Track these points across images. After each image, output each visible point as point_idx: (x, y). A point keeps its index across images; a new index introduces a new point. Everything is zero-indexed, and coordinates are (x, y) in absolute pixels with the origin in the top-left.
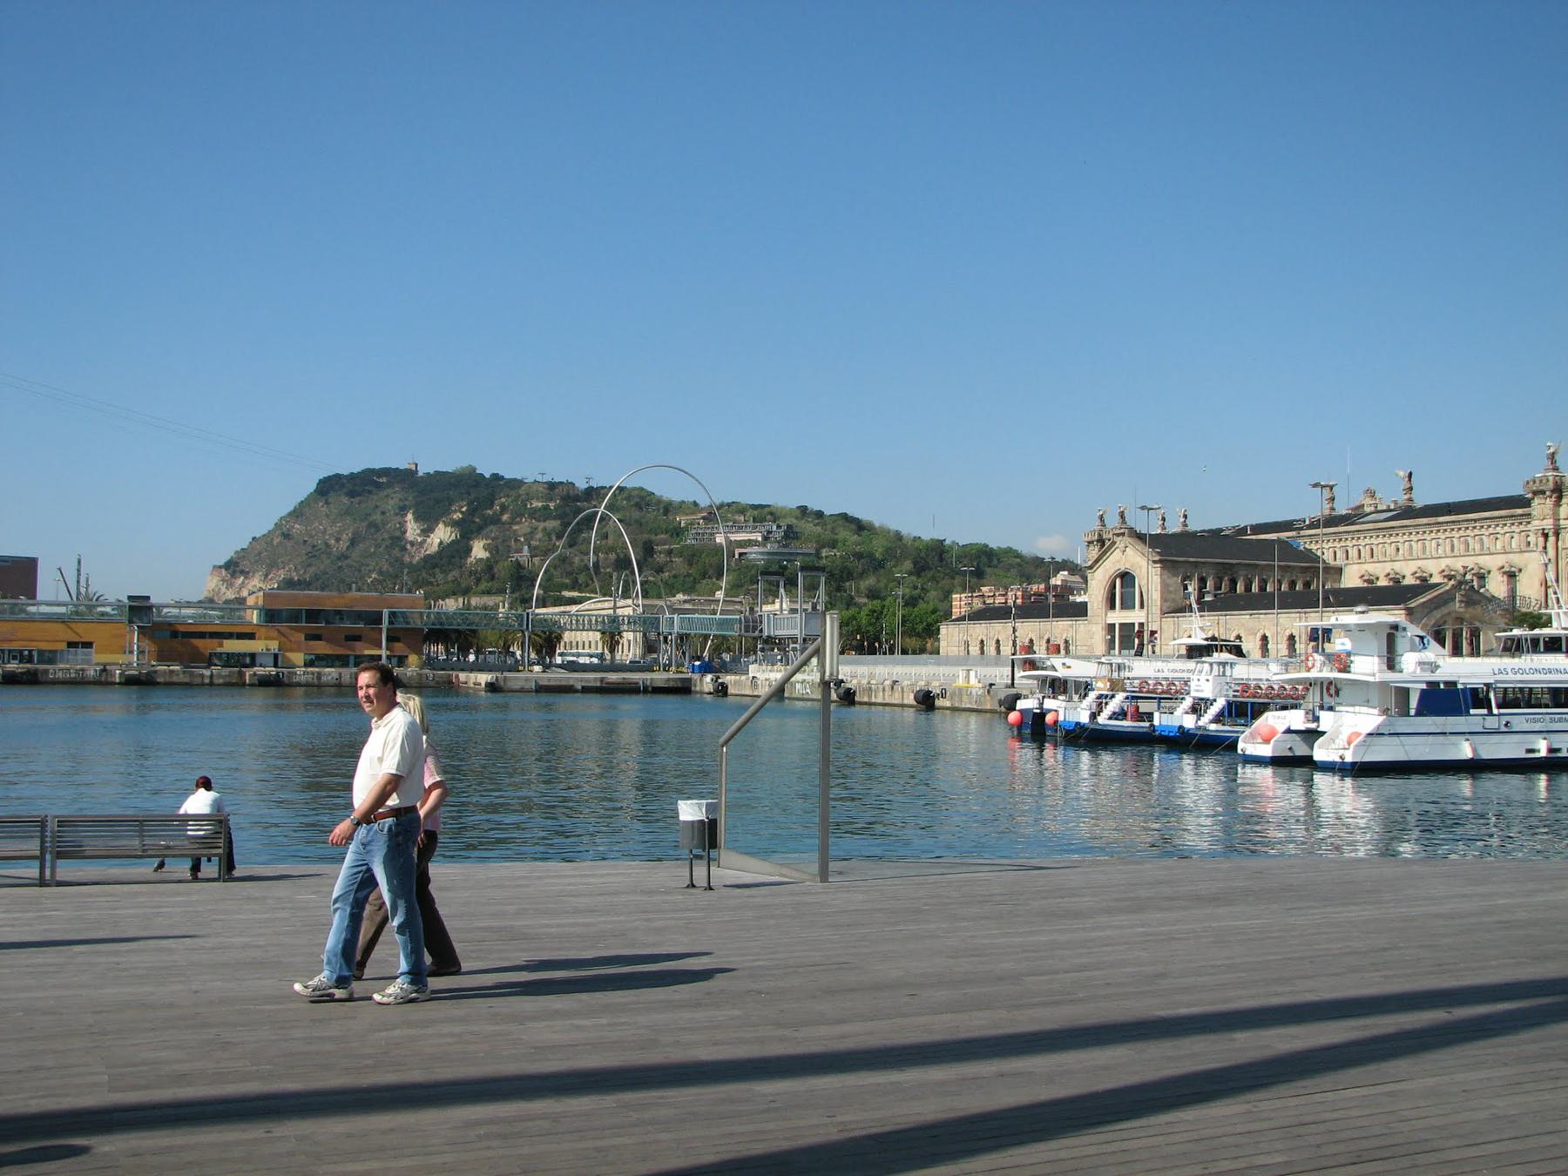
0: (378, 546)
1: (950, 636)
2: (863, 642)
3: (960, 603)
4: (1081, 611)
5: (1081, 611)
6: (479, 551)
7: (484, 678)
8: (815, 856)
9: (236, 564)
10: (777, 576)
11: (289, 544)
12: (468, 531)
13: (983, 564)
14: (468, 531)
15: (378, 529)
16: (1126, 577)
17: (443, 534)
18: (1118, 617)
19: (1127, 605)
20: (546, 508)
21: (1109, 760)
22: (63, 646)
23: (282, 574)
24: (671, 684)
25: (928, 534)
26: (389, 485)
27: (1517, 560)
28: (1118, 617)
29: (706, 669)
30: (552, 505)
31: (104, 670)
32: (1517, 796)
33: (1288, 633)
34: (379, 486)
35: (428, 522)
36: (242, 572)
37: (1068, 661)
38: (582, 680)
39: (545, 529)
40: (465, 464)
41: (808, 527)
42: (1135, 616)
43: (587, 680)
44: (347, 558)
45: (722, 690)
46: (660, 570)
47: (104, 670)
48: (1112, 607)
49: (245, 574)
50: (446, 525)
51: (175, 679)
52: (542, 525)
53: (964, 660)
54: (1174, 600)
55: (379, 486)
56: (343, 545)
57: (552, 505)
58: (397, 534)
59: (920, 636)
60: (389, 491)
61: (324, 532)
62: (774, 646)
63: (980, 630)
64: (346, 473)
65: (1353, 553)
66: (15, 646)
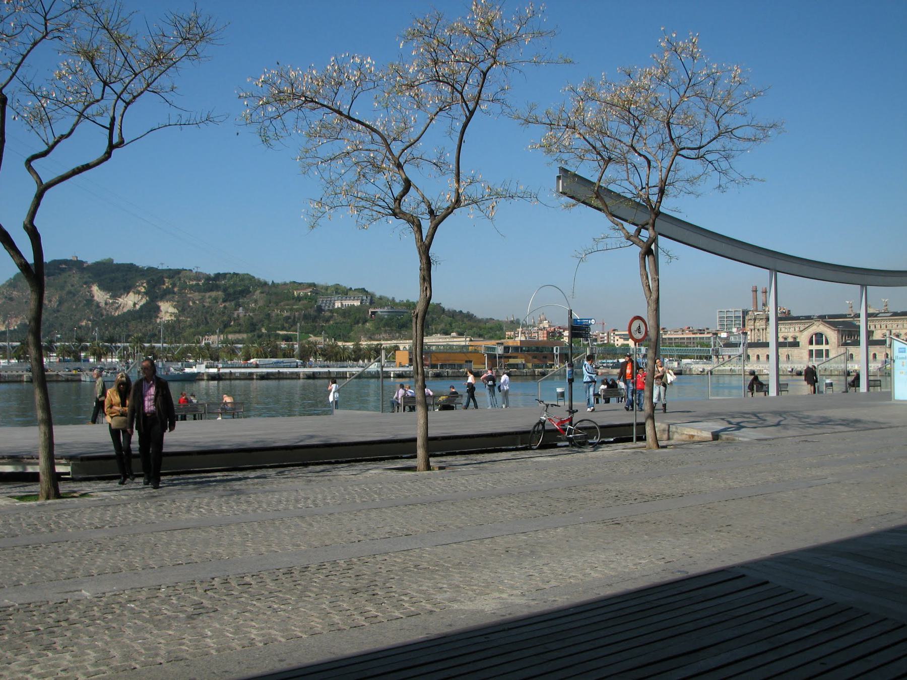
0: (77, 305)
8: (56, 441)
11: (13, 303)
15: (74, 295)
18: (814, 347)
19: (819, 342)
20: (198, 285)
22: (463, 362)
26: (70, 269)
28: (814, 347)
30: (201, 283)
32: (436, 414)
34: (63, 270)
39: (210, 297)
40: (107, 258)
42: (824, 347)
44: (58, 311)
46: (327, 321)
50: (135, 293)
52: (208, 295)
55: (63, 270)
57: (201, 283)
60: (69, 273)
65: (878, 326)
66: (451, 362)
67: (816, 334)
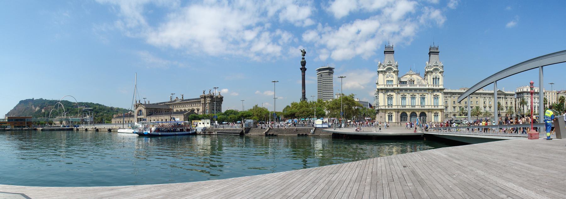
1: (113, 121)
2: (101, 122)
3: (114, 116)
4: (133, 116)
5: (133, 116)
6: (43, 111)
7: (41, 128)
10: (85, 113)
12: (41, 108)
13: (118, 110)
14: (41, 108)
16: (140, 111)
17: (37, 109)
18: (139, 117)
19: (141, 115)
21: (153, 140)
25: (110, 106)
27: (199, 107)
28: (139, 117)
29: (75, 126)
35: (35, 107)
41: (97, 107)
45: (78, 130)
53: (116, 124)
59: (109, 121)
62: (86, 123)
63: (118, 120)
64: (252, 108)
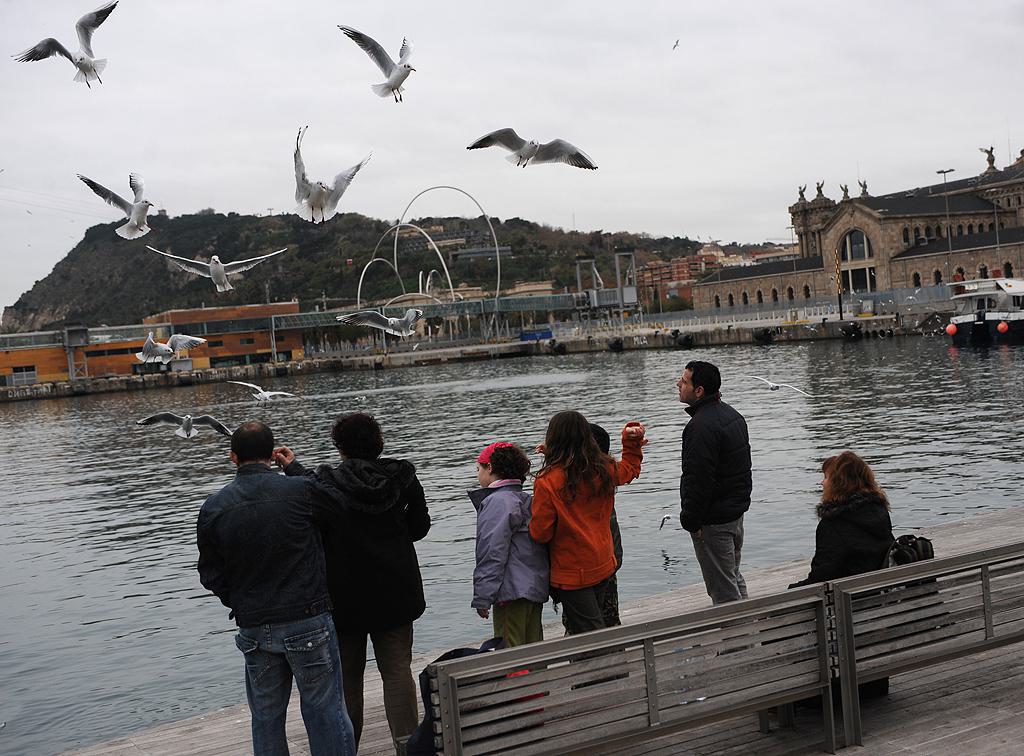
9: (26, 304)
15: (143, 266)
18: (849, 266)
19: (858, 255)
23: (67, 308)
24: (513, 350)
31: (259, 685)
33: (1004, 262)
36: (31, 310)
37: (1009, 281)
38: (445, 354)
40: (206, 208)
42: (866, 263)
43: (451, 354)
47: (259, 685)
48: (844, 258)
49: (36, 311)
51: (114, 387)
54: (897, 248)
56: (118, 279)
58: (160, 266)
61: (98, 271)
67: (851, 233)
